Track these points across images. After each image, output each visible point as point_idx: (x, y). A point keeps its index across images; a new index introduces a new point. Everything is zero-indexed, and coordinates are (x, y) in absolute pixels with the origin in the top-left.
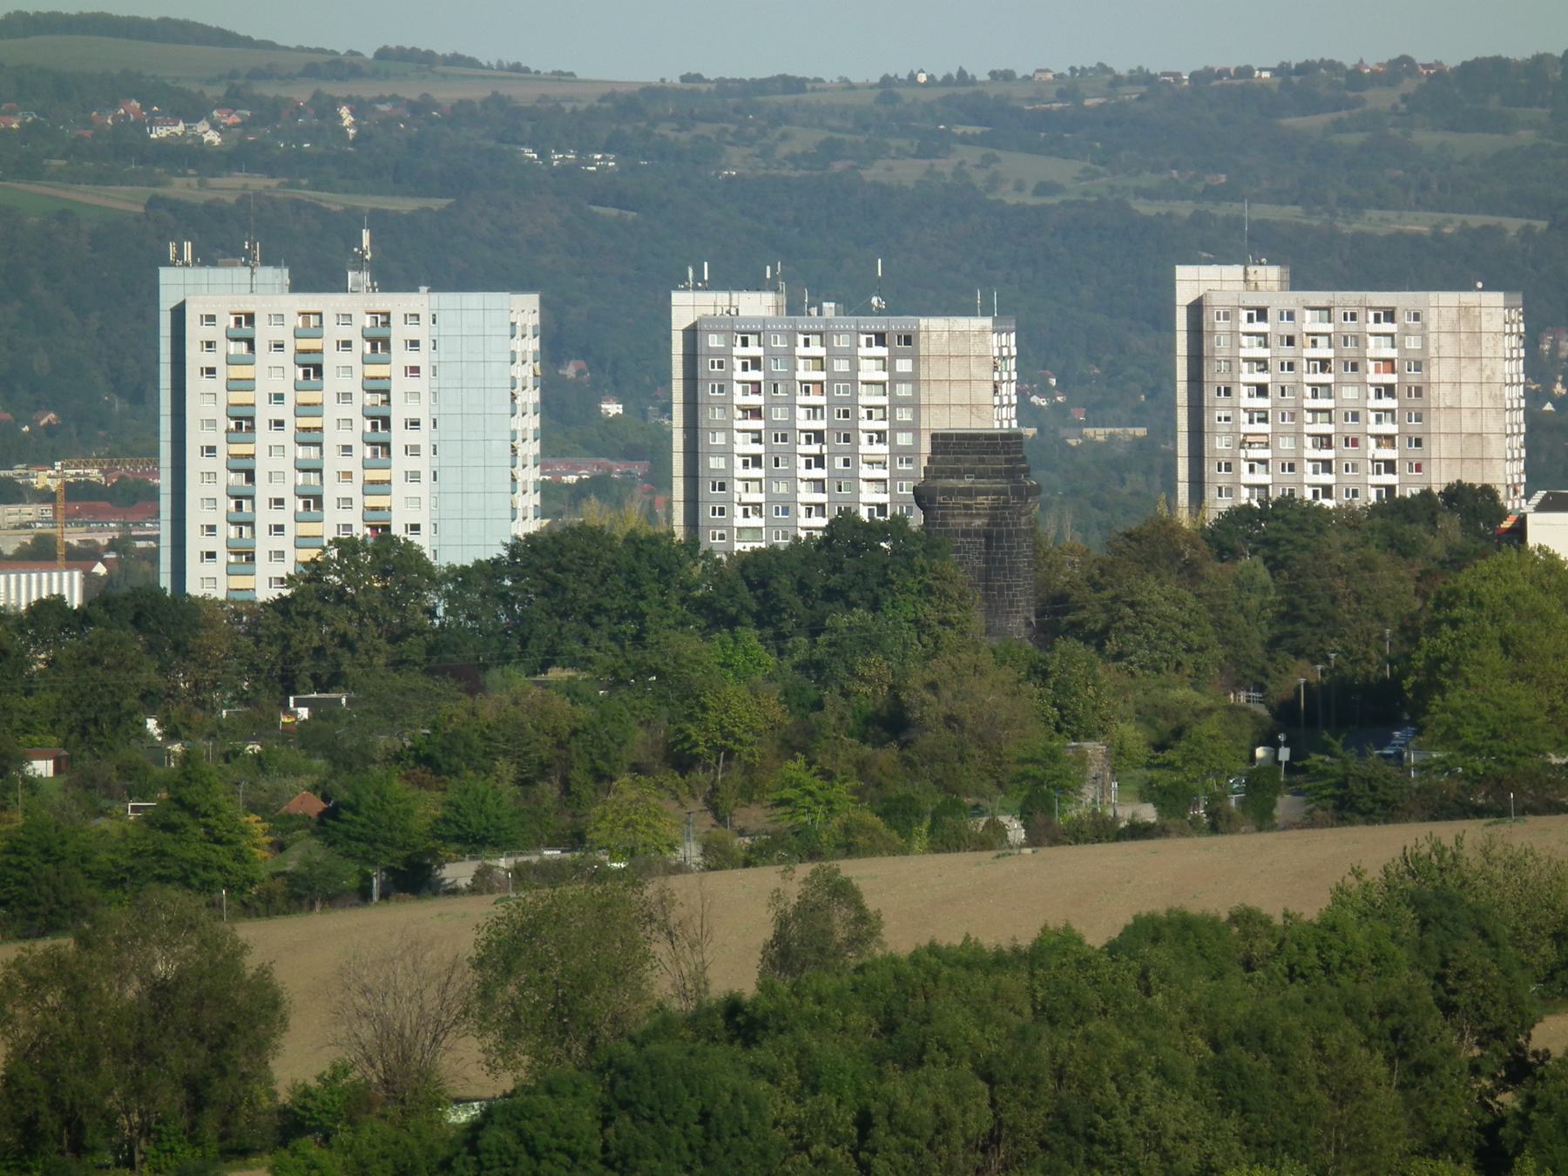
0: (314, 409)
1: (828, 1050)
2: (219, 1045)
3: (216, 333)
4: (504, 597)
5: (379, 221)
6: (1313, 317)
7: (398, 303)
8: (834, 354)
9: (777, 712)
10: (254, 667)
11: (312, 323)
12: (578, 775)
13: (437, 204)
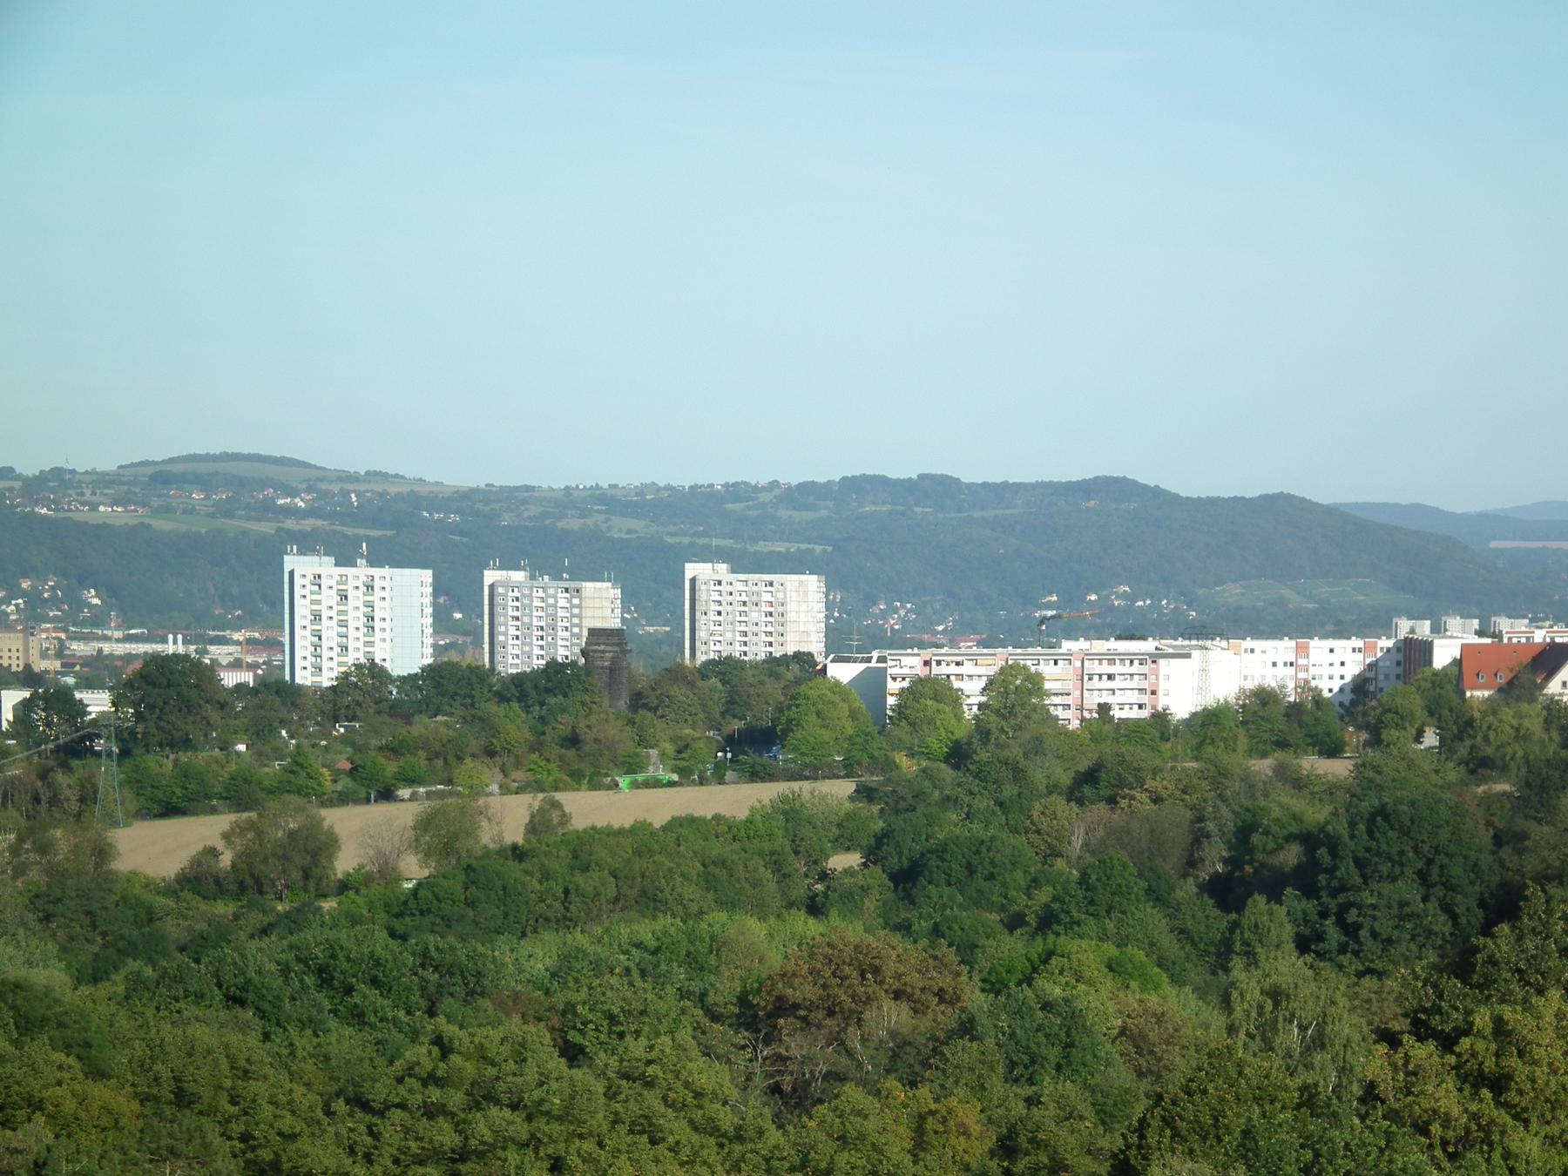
0: (344, 613)
1: (553, 865)
2: (315, 854)
3: (306, 582)
4: (420, 688)
5: (369, 540)
6: (741, 584)
7: (377, 572)
8: (548, 596)
9: (528, 735)
10: (323, 712)
11: (343, 579)
12: (451, 759)
13: (389, 533)
